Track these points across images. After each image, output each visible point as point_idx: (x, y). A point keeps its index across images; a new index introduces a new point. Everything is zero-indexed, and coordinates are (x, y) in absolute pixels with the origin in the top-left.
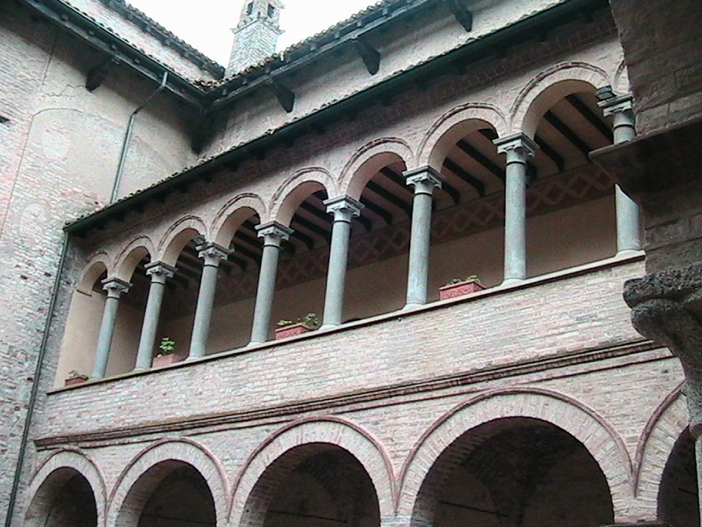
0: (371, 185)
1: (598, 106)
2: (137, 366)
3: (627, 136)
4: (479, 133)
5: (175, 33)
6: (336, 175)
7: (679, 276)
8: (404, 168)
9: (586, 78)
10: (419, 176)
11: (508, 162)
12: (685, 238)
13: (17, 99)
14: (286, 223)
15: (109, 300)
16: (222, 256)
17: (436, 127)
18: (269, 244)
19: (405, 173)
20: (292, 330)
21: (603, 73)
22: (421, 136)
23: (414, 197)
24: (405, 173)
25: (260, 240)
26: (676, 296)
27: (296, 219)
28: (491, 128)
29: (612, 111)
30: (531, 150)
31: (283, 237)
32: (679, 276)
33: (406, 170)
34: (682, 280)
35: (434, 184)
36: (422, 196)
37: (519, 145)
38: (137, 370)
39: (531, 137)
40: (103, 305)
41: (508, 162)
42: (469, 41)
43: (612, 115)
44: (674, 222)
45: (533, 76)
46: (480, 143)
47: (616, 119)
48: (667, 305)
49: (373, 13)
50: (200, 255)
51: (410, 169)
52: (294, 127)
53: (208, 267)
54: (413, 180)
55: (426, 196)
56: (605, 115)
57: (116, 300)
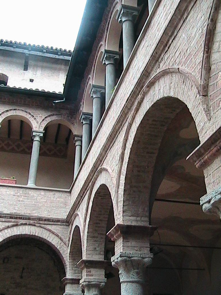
3: (103, 271)
7: (130, 254)
12: (130, 246)
15: (84, 126)
16: (101, 91)
17: (7, 111)
21: (123, 153)
26: (129, 257)
29: (36, 134)
30: (134, 12)
31: (115, 57)
32: (130, 254)
34: (131, 255)
35: (100, 92)
36: (78, 146)
40: (92, 108)
44: (128, 242)
48: (128, 259)
52: (38, 93)
53: (85, 125)
55: (97, 98)
56: (33, 134)
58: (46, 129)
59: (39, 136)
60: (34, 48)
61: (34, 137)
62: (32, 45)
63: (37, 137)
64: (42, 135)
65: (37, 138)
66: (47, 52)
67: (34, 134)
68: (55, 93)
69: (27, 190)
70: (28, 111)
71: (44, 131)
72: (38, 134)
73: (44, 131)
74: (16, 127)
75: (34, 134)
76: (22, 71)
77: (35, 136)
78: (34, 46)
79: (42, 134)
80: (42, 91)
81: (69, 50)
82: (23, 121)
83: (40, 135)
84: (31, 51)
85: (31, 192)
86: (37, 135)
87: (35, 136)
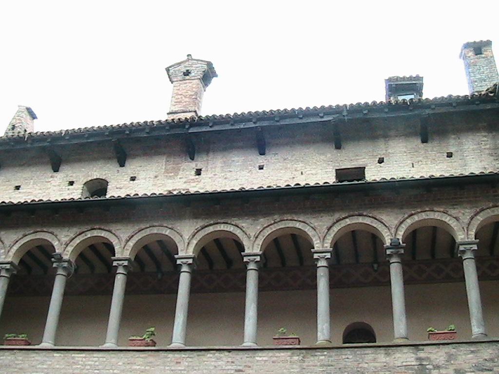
0: (29, 253)
1: (311, 251)
2: (173, 341)
4: (103, 244)
5: (455, 94)
6: (186, 237)
8: (176, 253)
9: (166, 232)
10: (324, 254)
11: (117, 272)
13: (197, 74)
14: (16, 262)
18: (4, 275)
19: (176, 256)
20: (449, 334)
22: (193, 230)
23: (56, 275)
24: (176, 256)
25: (113, 268)
27: (22, 262)
28: (108, 242)
33: (178, 254)
37: (126, 264)
38: (173, 346)
39: (133, 259)
41: (117, 272)
42: (382, 181)
43: (248, 262)
45: (277, 217)
46: (104, 251)
47: (320, 262)
49: (76, 134)
50: (55, 265)
51: (181, 254)
54: (182, 262)
56: (114, 265)
57: (64, 277)
58: (336, 245)
59: (470, 250)
60: (134, 128)
61: (317, 261)
62: (311, 108)
63: (251, 262)
64: (328, 255)
65: (322, 263)
66: (325, 114)
67: (316, 256)
68: (385, 180)
69: (343, 350)
70: (50, 230)
71: (332, 249)
72: (468, 247)
73: (332, 249)
74: (157, 250)
75: (316, 256)
76: (50, 173)
77: (247, 263)
78: (161, 123)
79: (329, 254)
80: (143, 196)
81: (227, 115)
82: (217, 239)
83: (255, 259)
84: (481, 105)
85: (113, 358)
86: (321, 258)
87: (463, 252)
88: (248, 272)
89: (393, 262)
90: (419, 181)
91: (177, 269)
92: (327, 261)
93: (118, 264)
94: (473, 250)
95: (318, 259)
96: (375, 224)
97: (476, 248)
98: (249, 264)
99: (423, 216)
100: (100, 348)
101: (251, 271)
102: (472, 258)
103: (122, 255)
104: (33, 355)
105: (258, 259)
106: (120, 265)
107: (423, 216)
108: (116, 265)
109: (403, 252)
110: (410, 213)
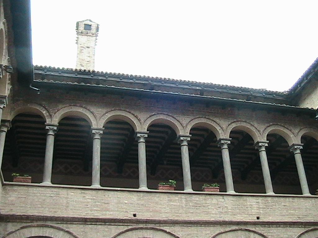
22: (189, 120)
54: (95, 132)
59: (226, 143)
67: (47, 127)
88: (222, 151)
89: (96, 138)
90: (177, 95)
91: (45, 134)
92: (145, 139)
93: (141, 135)
94: (145, 137)
95: (223, 143)
96: (214, 125)
97: (302, 148)
98: (224, 145)
99: (162, 117)
100: (41, 184)
101: (96, 140)
102: (187, 145)
103: (97, 126)
104: (225, 197)
105: (55, 128)
106: (225, 143)
107: (162, 117)
108: (140, 136)
109: (56, 129)
110: (150, 114)
